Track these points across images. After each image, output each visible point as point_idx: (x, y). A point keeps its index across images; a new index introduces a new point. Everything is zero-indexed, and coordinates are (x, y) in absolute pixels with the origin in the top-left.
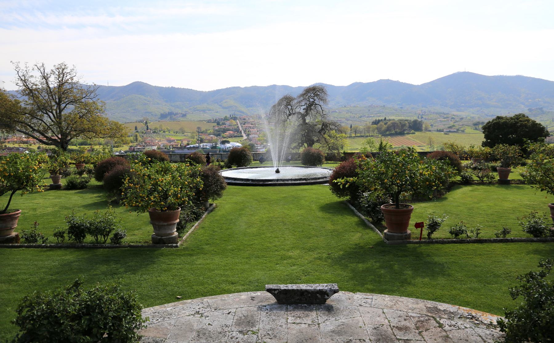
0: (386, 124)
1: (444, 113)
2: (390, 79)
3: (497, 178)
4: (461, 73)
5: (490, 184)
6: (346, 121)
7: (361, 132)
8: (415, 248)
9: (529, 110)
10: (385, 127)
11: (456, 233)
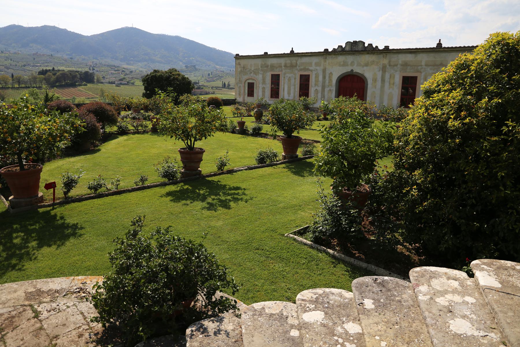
0: (54, 74)
1: (114, 66)
2: (57, 26)
3: (150, 126)
4: (129, 28)
5: (144, 132)
6: (6, 70)
7: (25, 83)
8: (48, 212)
9: (186, 66)
10: (53, 78)
11: (95, 188)
